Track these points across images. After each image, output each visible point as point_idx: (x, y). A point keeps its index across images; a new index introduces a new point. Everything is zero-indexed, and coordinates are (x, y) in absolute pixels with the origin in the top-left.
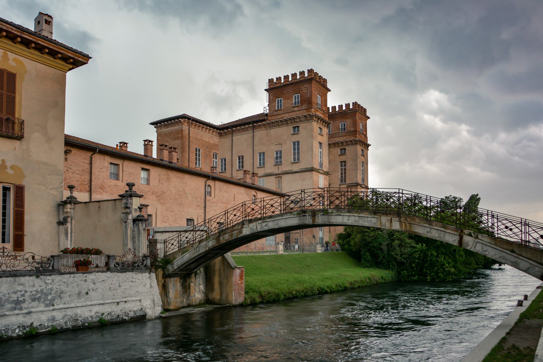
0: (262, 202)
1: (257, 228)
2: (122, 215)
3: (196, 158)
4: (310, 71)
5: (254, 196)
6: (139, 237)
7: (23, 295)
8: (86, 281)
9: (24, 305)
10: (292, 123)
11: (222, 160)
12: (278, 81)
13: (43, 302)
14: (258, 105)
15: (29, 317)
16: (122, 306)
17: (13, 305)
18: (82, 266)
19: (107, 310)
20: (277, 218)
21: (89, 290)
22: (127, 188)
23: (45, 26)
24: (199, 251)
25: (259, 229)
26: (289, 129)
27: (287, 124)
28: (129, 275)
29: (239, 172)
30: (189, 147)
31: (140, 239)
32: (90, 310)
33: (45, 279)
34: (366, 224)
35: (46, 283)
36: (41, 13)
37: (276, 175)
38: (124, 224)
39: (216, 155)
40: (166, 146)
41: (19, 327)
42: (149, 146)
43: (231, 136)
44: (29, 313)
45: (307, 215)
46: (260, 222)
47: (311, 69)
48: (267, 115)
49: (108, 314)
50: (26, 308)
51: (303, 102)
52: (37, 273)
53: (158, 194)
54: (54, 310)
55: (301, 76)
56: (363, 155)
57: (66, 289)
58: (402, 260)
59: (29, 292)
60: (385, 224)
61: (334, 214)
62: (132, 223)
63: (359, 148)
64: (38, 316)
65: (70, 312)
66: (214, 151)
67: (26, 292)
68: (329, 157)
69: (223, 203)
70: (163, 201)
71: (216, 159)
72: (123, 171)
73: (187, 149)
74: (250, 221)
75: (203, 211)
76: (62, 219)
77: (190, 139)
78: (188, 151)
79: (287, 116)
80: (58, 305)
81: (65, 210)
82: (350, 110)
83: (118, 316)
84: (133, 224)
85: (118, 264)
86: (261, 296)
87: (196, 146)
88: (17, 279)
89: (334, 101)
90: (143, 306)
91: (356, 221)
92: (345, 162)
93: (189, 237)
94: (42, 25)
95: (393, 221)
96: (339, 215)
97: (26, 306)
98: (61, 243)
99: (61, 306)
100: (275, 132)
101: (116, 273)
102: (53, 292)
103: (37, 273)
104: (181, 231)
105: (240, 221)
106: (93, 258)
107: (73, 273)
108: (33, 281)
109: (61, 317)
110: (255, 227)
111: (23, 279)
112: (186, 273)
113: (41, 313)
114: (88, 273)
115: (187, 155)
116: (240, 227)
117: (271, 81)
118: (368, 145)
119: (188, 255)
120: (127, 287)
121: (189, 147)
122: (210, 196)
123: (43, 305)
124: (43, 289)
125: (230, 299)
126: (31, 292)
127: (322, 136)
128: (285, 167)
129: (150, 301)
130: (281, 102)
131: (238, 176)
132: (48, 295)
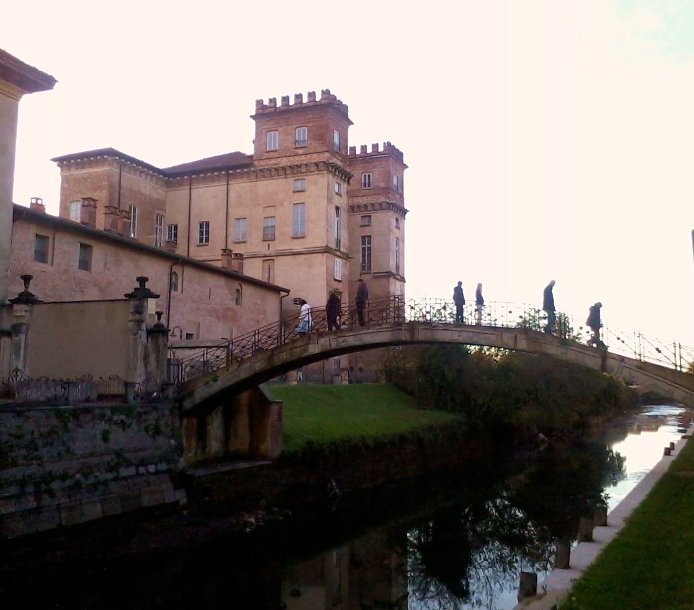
4: (326, 93)
5: (238, 290)
6: (189, 356)
12: (272, 105)
22: (137, 285)
25: (333, 346)
43: (188, 187)
48: (251, 157)
63: (391, 216)
66: (157, 212)
72: (53, 248)
79: (284, 162)
82: (379, 153)
87: (130, 203)
95: (518, 338)
104: (210, 347)
118: (405, 212)
127: (340, 196)
128: (281, 245)
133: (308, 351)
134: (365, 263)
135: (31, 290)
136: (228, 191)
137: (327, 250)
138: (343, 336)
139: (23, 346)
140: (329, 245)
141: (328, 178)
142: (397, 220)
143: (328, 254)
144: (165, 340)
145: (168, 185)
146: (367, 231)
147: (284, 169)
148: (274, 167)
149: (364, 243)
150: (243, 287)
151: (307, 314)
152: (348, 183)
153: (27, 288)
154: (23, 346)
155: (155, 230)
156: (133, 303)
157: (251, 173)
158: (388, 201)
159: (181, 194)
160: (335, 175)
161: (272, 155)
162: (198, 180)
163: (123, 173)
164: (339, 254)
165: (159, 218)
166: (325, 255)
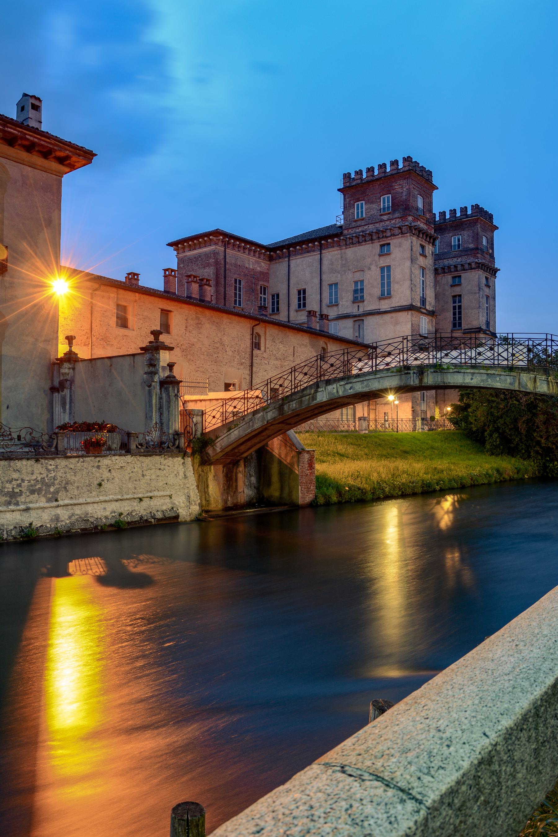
0: (346, 355)
1: (337, 392)
2: (145, 376)
3: (236, 294)
4: (407, 160)
7: (19, 485)
8: (98, 467)
9: (22, 499)
10: (379, 238)
11: (273, 296)
12: (358, 177)
13: (44, 496)
14: (330, 211)
15: (26, 514)
16: (146, 503)
17: (8, 499)
18: (93, 448)
19: (126, 509)
20: (367, 378)
21: (103, 480)
22: (152, 338)
23: (32, 113)
24: (253, 426)
26: (376, 247)
27: (372, 239)
28: (156, 459)
29: (300, 313)
30: (225, 278)
31: (171, 409)
32: (105, 509)
33: (47, 464)
34: (498, 385)
35: (48, 470)
36: (25, 95)
37: (355, 316)
38: (147, 388)
39: (265, 288)
40: (195, 277)
41: (15, 527)
42: (171, 278)
43: (287, 259)
44: (27, 509)
45: (412, 372)
46: (342, 383)
47: (409, 157)
48: (341, 227)
49: (128, 514)
50: (25, 503)
51: (396, 206)
52: (36, 455)
53: (184, 347)
54: (58, 506)
55: (393, 167)
56: (488, 286)
57: (73, 478)
58: (550, 445)
59: (26, 482)
60: (527, 385)
61: (451, 371)
62: (158, 388)
64: (38, 514)
65: (78, 511)
66: (261, 283)
67: (23, 480)
68: (435, 289)
69: (277, 359)
70: (191, 358)
71: (265, 294)
73: (223, 280)
74: (328, 382)
75: (247, 372)
76: (56, 383)
77: (227, 266)
78: (223, 283)
80: (62, 500)
81: (63, 371)
83: (141, 518)
84: (161, 389)
85: (141, 445)
86: (340, 493)
87: (235, 276)
88: (12, 463)
89: (443, 203)
90: (174, 504)
91: (483, 381)
92: (460, 296)
93: (238, 407)
94: (28, 112)
95: (538, 380)
96: (458, 372)
97: (23, 500)
98: (56, 417)
99: (67, 502)
100: (353, 253)
101: (138, 457)
102: (56, 482)
103: (36, 455)
105: (311, 383)
106: (104, 436)
107: (82, 456)
108: (31, 466)
109: (67, 517)
110: (335, 391)
111: (18, 464)
112: (231, 461)
113: (41, 510)
114: (101, 457)
115: (223, 290)
116: (313, 391)
117: (347, 176)
119: (236, 432)
120: (153, 477)
121: (225, 278)
122: (259, 349)
123: (43, 499)
124: (44, 478)
125: (294, 497)
126: (29, 481)
127: (426, 257)
128: (369, 305)
129: (184, 496)
130: (362, 208)
131: (300, 318)
132: (50, 486)
133: (316, 399)
134: (456, 320)
135: (74, 349)
136: (321, 259)
137: (410, 308)
138: (351, 383)
139: (68, 400)
140: (414, 304)
141: (412, 239)
142: (487, 278)
143: (413, 312)
144: (176, 389)
145: (271, 259)
146: (457, 290)
147: (370, 234)
148: (361, 234)
149: (454, 302)
150: (328, 345)
151: (378, 365)
152: (434, 244)
153: (70, 347)
154: (68, 400)
155: (259, 299)
156: (148, 356)
157: (341, 241)
158: (476, 260)
159: (280, 268)
160: (418, 236)
161: (359, 223)
162: (296, 253)
163: (228, 250)
164: (424, 311)
165: (264, 290)
166: (410, 312)
